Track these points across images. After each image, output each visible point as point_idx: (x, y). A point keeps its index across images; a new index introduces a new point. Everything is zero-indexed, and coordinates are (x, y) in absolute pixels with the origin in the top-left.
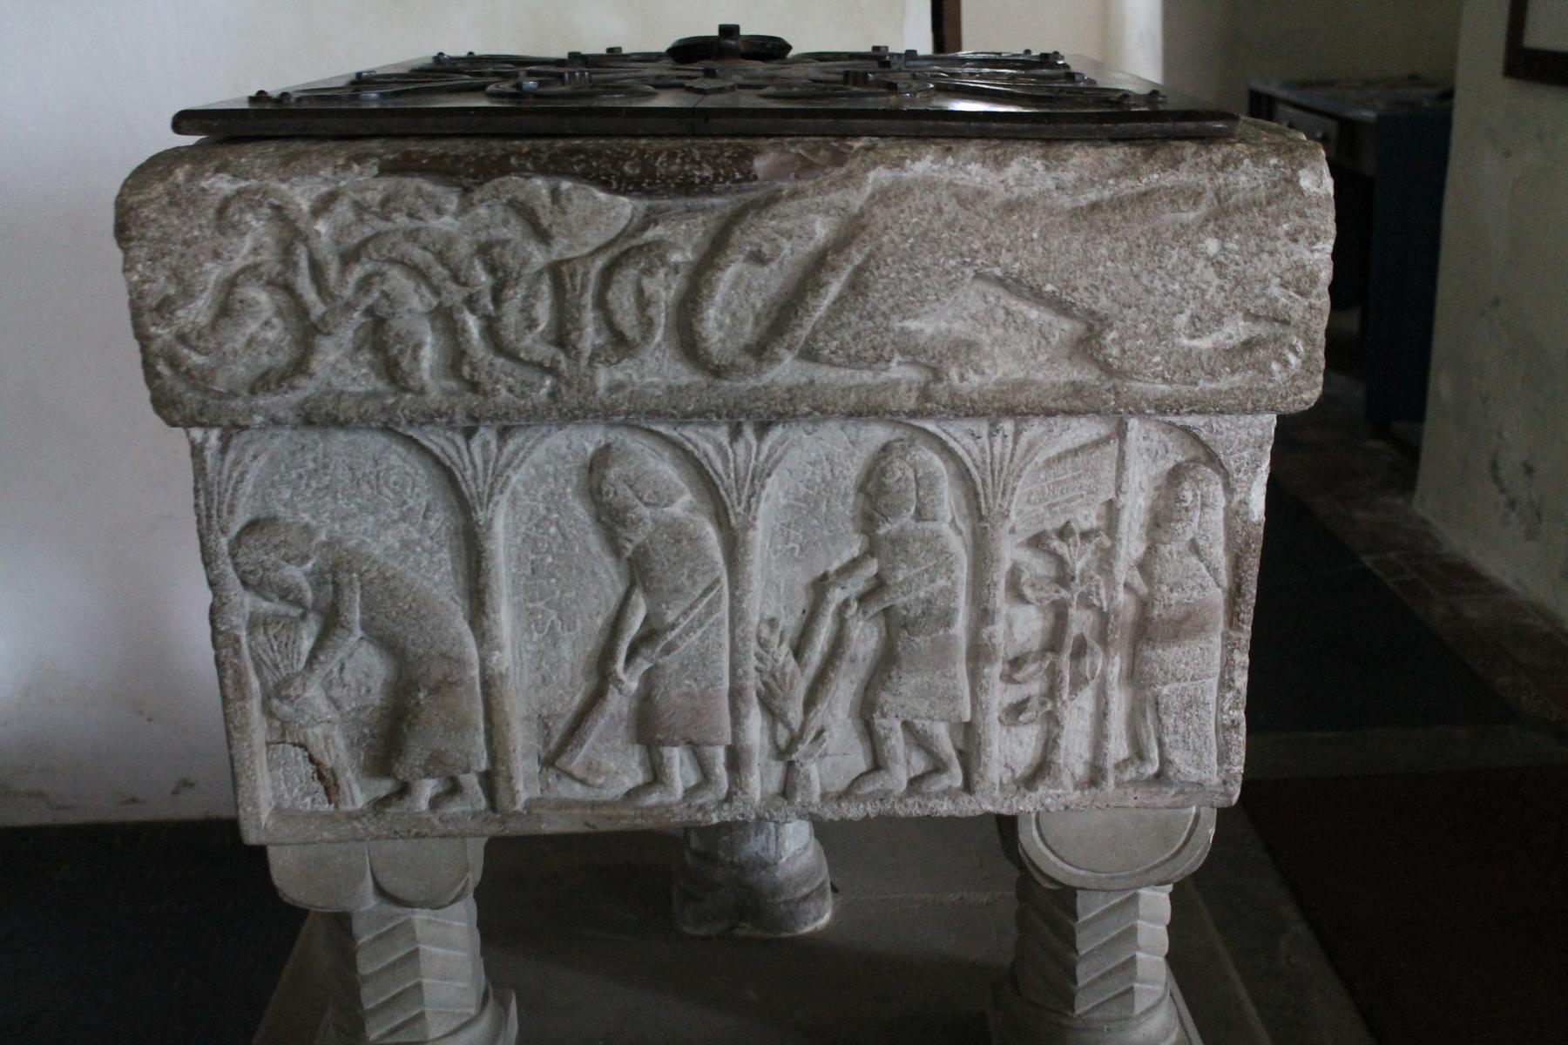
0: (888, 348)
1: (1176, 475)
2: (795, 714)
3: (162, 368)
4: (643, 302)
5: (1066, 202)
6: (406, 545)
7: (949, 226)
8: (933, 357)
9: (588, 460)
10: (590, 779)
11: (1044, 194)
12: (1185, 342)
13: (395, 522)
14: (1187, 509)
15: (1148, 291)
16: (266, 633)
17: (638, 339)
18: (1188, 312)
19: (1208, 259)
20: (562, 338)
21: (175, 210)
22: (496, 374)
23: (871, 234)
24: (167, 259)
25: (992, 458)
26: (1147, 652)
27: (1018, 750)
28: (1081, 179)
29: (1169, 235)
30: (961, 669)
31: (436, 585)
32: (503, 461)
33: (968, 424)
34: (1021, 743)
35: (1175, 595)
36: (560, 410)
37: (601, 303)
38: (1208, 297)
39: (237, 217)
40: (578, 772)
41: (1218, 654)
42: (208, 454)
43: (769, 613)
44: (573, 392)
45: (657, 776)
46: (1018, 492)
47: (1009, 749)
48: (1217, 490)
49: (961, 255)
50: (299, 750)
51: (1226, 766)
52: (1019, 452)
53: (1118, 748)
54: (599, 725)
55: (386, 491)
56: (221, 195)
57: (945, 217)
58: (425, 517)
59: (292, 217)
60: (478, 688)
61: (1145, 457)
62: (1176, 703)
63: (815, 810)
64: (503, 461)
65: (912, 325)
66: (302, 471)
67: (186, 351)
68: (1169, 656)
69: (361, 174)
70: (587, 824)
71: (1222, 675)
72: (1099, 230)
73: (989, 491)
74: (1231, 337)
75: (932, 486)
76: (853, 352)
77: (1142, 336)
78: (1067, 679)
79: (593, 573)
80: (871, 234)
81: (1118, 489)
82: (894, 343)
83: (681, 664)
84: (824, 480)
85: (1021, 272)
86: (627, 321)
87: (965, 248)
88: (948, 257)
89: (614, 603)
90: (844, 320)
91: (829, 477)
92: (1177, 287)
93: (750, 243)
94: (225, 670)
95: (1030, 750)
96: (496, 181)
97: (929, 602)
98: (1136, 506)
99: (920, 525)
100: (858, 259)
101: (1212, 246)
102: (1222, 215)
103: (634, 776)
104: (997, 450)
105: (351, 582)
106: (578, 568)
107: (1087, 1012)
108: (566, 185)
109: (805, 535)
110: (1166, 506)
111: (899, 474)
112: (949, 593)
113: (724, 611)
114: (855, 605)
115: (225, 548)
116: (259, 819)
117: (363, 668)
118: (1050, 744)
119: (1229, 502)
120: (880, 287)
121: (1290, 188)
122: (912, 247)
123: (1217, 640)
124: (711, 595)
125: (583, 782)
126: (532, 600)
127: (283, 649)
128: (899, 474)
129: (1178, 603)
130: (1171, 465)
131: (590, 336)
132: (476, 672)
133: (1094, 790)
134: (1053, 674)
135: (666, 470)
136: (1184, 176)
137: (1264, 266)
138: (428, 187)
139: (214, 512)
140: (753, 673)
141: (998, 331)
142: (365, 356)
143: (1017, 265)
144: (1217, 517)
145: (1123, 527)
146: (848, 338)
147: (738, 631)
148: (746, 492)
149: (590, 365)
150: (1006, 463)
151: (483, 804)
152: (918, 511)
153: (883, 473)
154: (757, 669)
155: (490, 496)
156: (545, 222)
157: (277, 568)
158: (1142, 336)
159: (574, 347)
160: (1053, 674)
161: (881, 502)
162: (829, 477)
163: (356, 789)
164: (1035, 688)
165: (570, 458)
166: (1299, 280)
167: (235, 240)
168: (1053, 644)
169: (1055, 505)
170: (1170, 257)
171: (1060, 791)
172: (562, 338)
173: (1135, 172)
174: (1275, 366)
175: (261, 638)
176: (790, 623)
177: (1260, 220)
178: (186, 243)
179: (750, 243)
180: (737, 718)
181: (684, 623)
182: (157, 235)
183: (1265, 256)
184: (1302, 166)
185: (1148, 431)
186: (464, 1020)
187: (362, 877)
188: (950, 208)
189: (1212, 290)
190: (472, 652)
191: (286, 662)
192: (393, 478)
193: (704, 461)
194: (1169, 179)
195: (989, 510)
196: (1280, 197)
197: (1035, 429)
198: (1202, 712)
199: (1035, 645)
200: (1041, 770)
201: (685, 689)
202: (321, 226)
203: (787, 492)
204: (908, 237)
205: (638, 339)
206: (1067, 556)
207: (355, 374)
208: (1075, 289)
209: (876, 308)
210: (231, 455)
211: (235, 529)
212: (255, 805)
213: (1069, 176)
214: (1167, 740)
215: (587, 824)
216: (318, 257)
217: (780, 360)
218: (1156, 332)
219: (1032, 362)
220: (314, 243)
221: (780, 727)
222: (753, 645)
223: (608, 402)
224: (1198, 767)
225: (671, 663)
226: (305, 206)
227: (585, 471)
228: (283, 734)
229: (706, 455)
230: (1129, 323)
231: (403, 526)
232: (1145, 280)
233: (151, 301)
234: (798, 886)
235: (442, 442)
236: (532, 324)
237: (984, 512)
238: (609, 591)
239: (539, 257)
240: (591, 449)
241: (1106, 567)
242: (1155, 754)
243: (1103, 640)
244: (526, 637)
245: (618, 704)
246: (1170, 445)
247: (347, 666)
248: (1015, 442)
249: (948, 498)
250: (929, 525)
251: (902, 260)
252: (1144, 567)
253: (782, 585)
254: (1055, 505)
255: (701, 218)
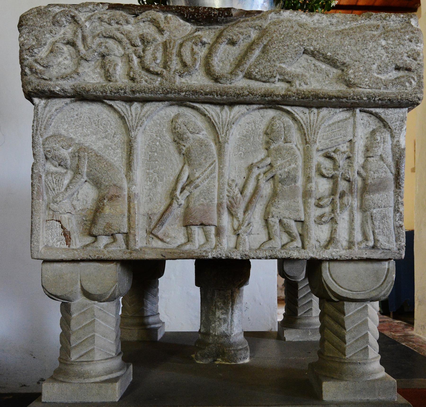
0: (275, 72)
1: (373, 132)
2: (240, 214)
3: (27, 70)
4: (193, 53)
5: (333, 28)
6: (106, 146)
7: (296, 32)
8: (290, 77)
9: (171, 119)
10: (165, 239)
11: (327, 26)
12: (376, 75)
13: (103, 138)
14: (378, 143)
15: (363, 56)
16: (51, 176)
17: (191, 65)
18: (376, 64)
19: (382, 46)
20: (165, 66)
21: (39, 16)
22: (142, 76)
23: (269, 33)
24: (34, 32)
25: (310, 121)
26: (367, 197)
27: (321, 234)
28: (338, 22)
29: (368, 38)
30: (300, 200)
31: (115, 161)
32: (142, 115)
33: (301, 109)
34: (322, 231)
35: (376, 175)
36: (163, 89)
37: (180, 55)
38: (383, 59)
39: (59, 18)
40: (160, 236)
41: (393, 198)
42: (40, 107)
43: (232, 178)
44: (168, 83)
45: (189, 239)
46: (319, 135)
47: (319, 233)
48: (388, 136)
49: (300, 41)
50: (58, 223)
51: (399, 243)
52: (319, 120)
53: (358, 237)
54: (170, 220)
55: (101, 127)
56: (55, 13)
57: (294, 29)
58: (113, 137)
59: (77, 20)
60: (126, 199)
61: (362, 126)
62: (379, 217)
63: (247, 253)
64: (142, 115)
65: (283, 66)
66: (72, 119)
67: (36, 64)
68: (374, 198)
69: (102, 8)
70: (162, 255)
71: (395, 207)
72: (345, 35)
73: (309, 133)
74: (391, 76)
75: (289, 130)
76: (263, 73)
77: (361, 71)
78: (339, 205)
79: (171, 160)
80: (269, 33)
81: (354, 136)
82: (277, 70)
83: (200, 192)
84: (252, 129)
85: (320, 48)
86: (188, 59)
87: (301, 39)
88: (295, 42)
89: (177, 171)
90: (260, 62)
91: (254, 128)
92: (372, 55)
93: (229, 35)
94: (34, 188)
95: (326, 234)
96: (147, 12)
97: (289, 172)
98: (360, 144)
99: (286, 145)
100: (265, 42)
101: (384, 43)
102: (386, 33)
103: (182, 239)
104: (312, 119)
105: (84, 156)
106: (166, 158)
107: (350, 357)
108: (169, 15)
109: (245, 149)
110: (371, 143)
111: (278, 125)
112: (295, 169)
113: (216, 174)
114: (263, 175)
115: (41, 142)
116: (39, 248)
117: (87, 194)
118: (333, 231)
119: (393, 142)
120: (273, 51)
121: (408, 25)
122: (283, 38)
123: (392, 193)
124: (212, 166)
125: (162, 240)
126: (149, 169)
127: (57, 182)
128: (278, 125)
129: (378, 177)
130: (371, 130)
131: (175, 64)
132: (126, 193)
133: (350, 250)
134: (333, 202)
135: (199, 121)
136: (373, 22)
137: (401, 49)
138: (124, 13)
139: (39, 128)
140: (226, 197)
141: (312, 73)
142: (98, 70)
143: (318, 46)
144: (388, 146)
145: (356, 149)
146: (262, 68)
147: (221, 181)
148: (225, 129)
149: (174, 73)
150: (315, 123)
151: (124, 246)
152: (285, 139)
153: (273, 125)
154: (228, 196)
155: (137, 127)
156: (162, 26)
157: (59, 149)
158: (361, 71)
159: (169, 67)
160: (333, 202)
161: (272, 136)
162: (254, 128)
163: (77, 240)
164: (327, 210)
165: (165, 118)
166: (413, 54)
167: (58, 28)
168: (333, 192)
169: (332, 140)
170: (369, 45)
171: (338, 250)
172: (165, 66)
173: (356, 20)
174: (407, 84)
175: (50, 178)
176: (240, 182)
177: (399, 34)
178: (41, 27)
179: (229, 35)
180: (220, 215)
181: (202, 177)
182: (32, 24)
183: (401, 46)
184: (411, 17)
185: (363, 117)
186: (110, 357)
187: (77, 283)
188: (296, 27)
189: (384, 57)
190: (125, 185)
191: (58, 188)
192: (104, 122)
193: (211, 118)
194: (367, 22)
195: (309, 139)
196: (405, 28)
197: (324, 112)
198: (388, 220)
199: (327, 193)
200: (331, 241)
201: (201, 202)
202: (87, 24)
203: (239, 133)
204: (282, 35)
205: (191, 65)
206: (337, 158)
207: (93, 77)
208: (338, 54)
209: (271, 58)
210: (48, 109)
211: (45, 136)
212: (38, 242)
213: (334, 21)
214: (376, 231)
215: (162, 255)
216: (85, 34)
217: (238, 75)
218: (366, 70)
219: (324, 83)
220: (84, 28)
221: (235, 220)
222: (226, 187)
223: (179, 86)
224: (388, 242)
225: (196, 192)
226: (83, 19)
227: (170, 122)
228: (53, 217)
229: (212, 116)
230: (356, 67)
231: (106, 140)
232: (361, 52)
233: (27, 47)
234: (238, 345)
235: (122, 107)
236: (155, 59)
237: (308, 140)
238: (176, 166)
239: (160, 39)
240: (173, 115)
241: (351, 165)
242: (372, 238)
243: (351, 191)
244: (146, 183)
245: (177, 211)
246: (371, 122)
247: (80, 192)
248: (318, 116)
249: (295, 137)
250: (288, 145)
251: (280, 42)
252: (363, 167)
253: (237, 167)
254: (332, 140)
255: (213, 30)
